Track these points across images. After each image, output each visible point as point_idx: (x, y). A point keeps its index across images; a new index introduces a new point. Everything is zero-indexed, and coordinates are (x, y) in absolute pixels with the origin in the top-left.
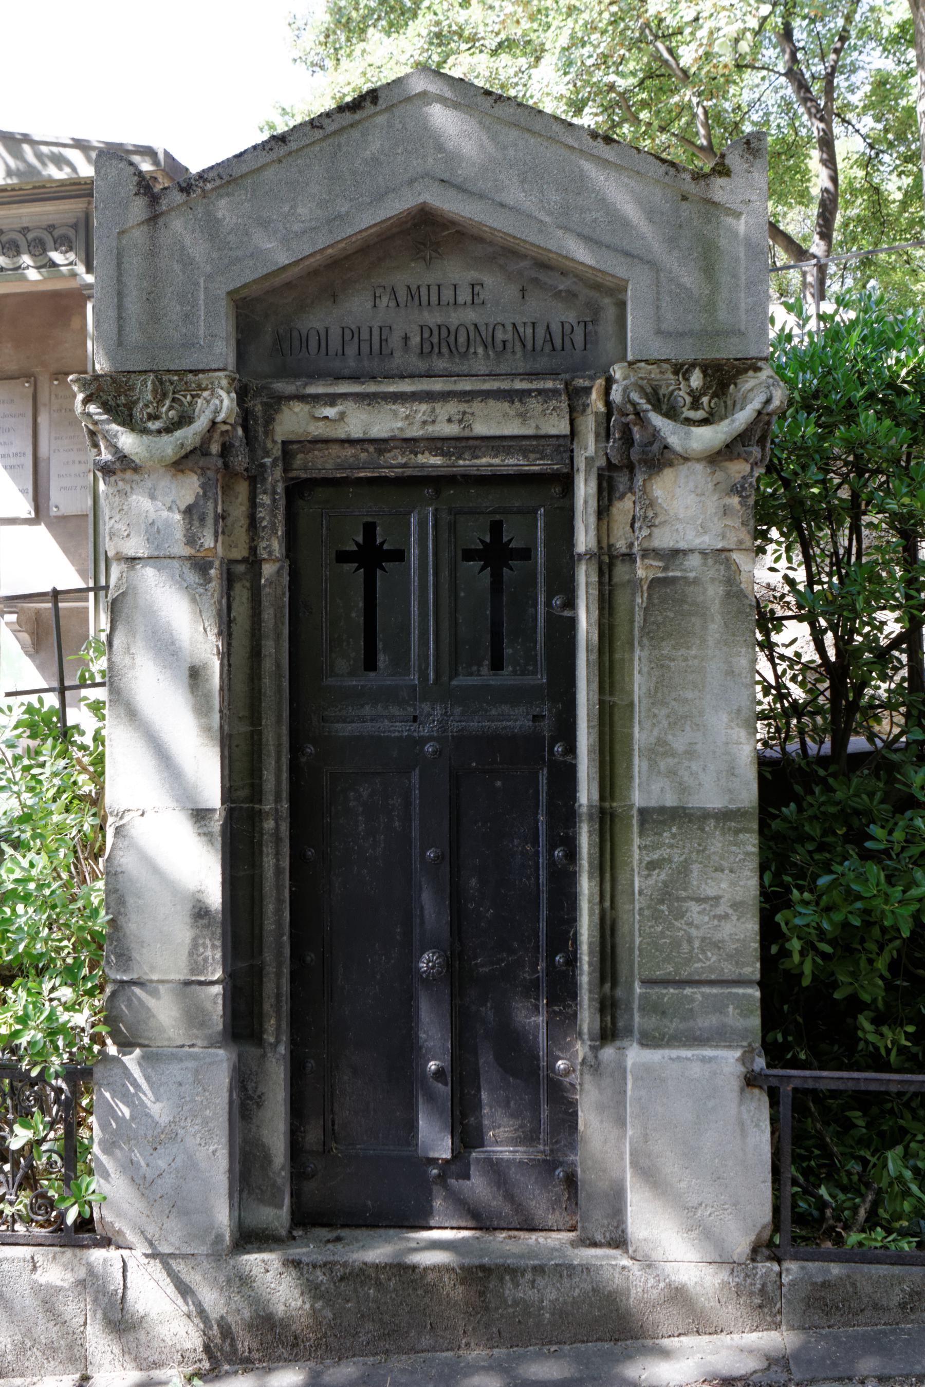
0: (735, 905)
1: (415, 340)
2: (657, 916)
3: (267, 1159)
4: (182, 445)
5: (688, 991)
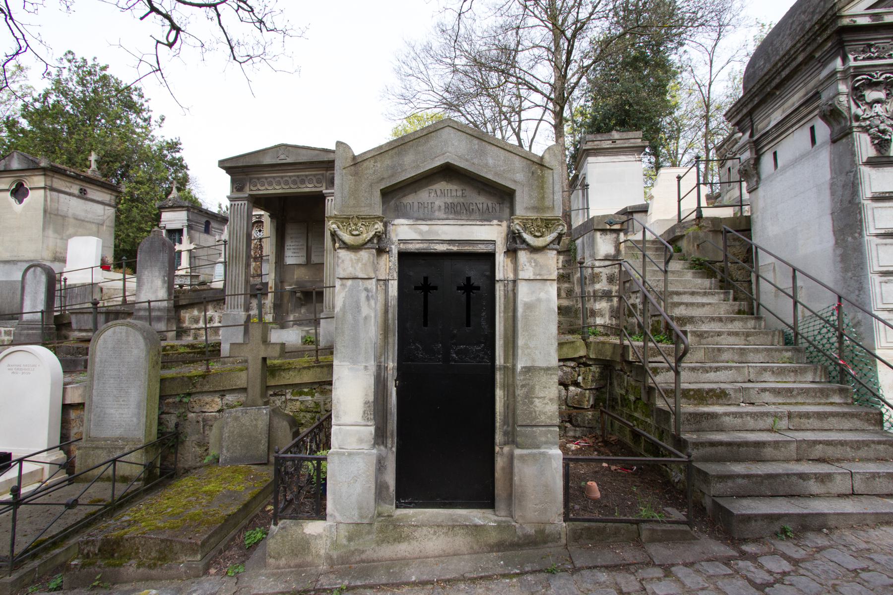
0: (551, 400)
1: (443, 207)
2: (524, 403)
3: (388, 488)
4: (131, 106)
5: (535, 429)
